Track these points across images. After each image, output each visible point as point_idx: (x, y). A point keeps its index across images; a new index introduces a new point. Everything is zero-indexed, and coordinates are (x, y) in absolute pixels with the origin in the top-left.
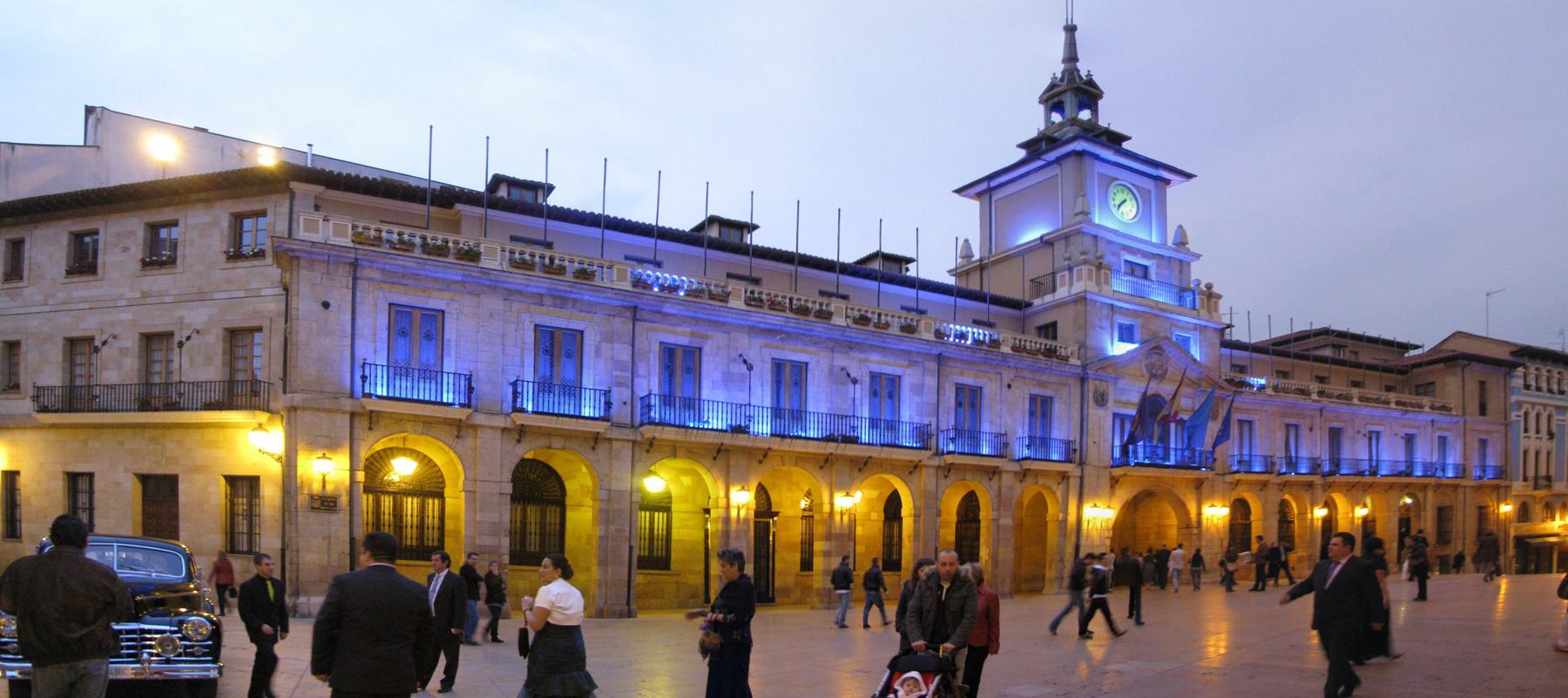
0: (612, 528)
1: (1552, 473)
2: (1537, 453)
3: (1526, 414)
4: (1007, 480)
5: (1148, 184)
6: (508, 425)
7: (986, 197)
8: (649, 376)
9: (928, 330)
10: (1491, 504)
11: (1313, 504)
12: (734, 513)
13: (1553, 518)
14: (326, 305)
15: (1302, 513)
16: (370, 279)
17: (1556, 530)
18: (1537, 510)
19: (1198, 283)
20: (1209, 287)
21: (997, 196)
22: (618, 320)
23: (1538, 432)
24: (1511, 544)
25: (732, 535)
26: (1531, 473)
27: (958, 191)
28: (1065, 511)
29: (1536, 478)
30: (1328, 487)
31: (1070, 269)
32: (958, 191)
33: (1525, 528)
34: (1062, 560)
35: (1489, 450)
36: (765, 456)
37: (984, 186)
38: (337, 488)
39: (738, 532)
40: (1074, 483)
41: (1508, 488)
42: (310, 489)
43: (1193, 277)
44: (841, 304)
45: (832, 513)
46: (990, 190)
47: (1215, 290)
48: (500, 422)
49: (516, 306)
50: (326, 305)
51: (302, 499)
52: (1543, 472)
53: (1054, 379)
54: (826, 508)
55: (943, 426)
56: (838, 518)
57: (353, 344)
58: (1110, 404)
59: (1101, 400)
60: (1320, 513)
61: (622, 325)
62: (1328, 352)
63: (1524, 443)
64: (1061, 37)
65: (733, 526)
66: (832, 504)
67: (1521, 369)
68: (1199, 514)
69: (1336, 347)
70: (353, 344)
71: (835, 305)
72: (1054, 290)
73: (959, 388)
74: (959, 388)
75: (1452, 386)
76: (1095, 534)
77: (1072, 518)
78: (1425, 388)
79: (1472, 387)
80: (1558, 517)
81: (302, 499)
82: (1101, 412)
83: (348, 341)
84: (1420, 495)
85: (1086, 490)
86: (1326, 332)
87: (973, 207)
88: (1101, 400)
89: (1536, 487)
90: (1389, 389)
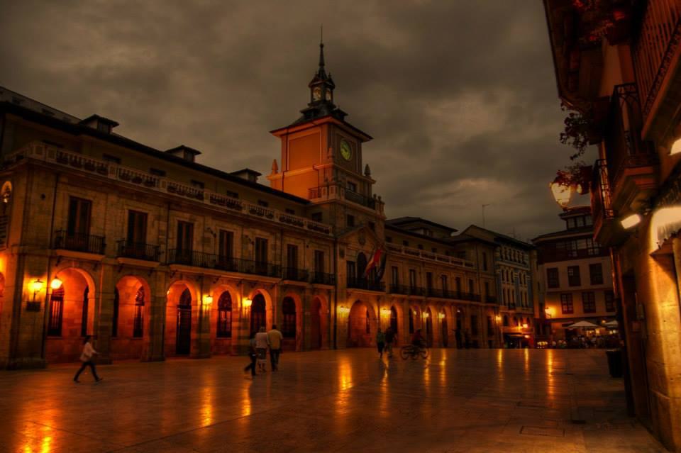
0: (156, 316)
1: (515, 302)
2: (509, 291)
3: (520, 275)
4: (308, 293)
5: (355, 141)
6: (117, 264)
7: (285, 137)
8: (173, 238)
9: (163, 186)
10: (492, 315)
11: (423, 310)
12: (204, 308)
13: (517, 325)
14: (43, 197)
15: (418, 315)
16: (64, 183)
17: (520, 331)
18: (511, 320)
19: (375, 196)
20: (380, 198)
21: (290, 138)
22: (162, 209)
23: (508, 280)
24: (502, 336)
25: (203, 319)
26: (507, 302)
27: (273, 132)
28: (330, 308)
29: (509, 304)
30: (428, 302)
31: (328, 186)
32: (273, 132)
33: (507, 329)
34: (329, 333)
35: (462, 282)
36: (217, 279)
37: (285, 132)
38: (40, 299)
39: (206, 317)
40: (333, 294)
41: (498, 308)
42: (28, 299)
43: (373, 194)
44: (115, 166)
45: (241, 308)
46: (288, 134)
47: (382, 200)
48: (113, 262)
49: (122, 200)
50: (43, 197)
51: (24, 304)
52: (511, 301)
53: (323, 243)
54: (239, 306)
55: (283, 266)
56: (244, 310)
57: (53, 219)
58: (346, 257)
59: (342, 255)
60: (425, 315)
61: (163, 211)
62: (422, 232)
63: (503, 286)
64: (319, 48)
65: (204, 314)
66: (241, 304)
67: (499, 248)
68: (379, 313)
69: (425, 229)
70: (53, 219)
71: (112, 165)
72: (320, 197)
73: (289, 246)
74: (289, 246)
75: (474, 254)
76: (342, 320)
77: (333, 312)
78: (461, 255)
79: (480, 255)
80: (519, 325)
81: (24, 304)
82: (342, 261)
83: (51, 217)
84: (464, 309)
85: (338, 299)
86: (419, 220)
87: (277, 143)
88: (342, 255)
89: (510, 309)
90: (447, 254)
